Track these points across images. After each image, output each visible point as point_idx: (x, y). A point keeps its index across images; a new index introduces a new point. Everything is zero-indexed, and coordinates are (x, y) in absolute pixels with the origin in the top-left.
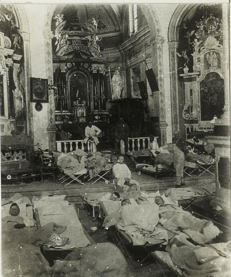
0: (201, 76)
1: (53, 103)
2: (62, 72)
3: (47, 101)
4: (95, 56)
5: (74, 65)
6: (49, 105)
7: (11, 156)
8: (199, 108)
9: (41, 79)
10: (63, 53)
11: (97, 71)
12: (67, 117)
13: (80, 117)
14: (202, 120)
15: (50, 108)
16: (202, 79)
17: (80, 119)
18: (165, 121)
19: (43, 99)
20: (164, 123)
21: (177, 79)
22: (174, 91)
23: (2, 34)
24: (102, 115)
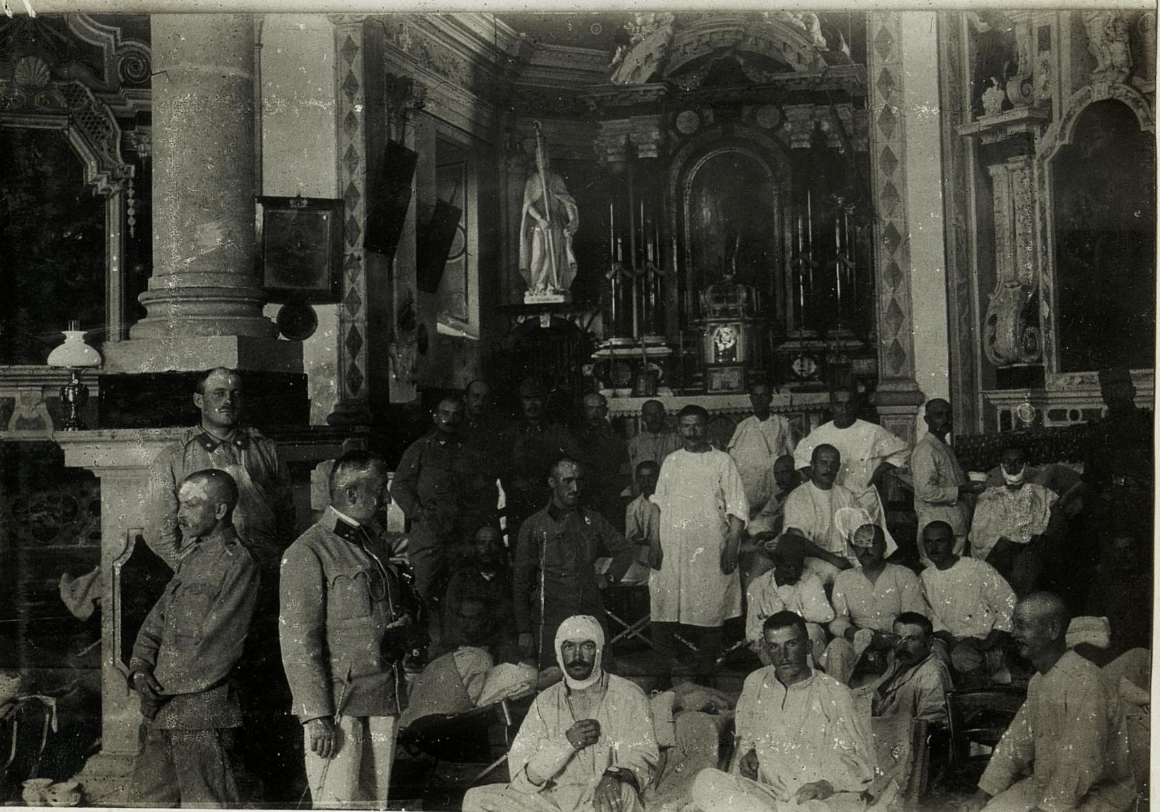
0: (1055, 127)
1: (363, 305)
2: (644, 159)
3: (334, 295)
4: (797, 66)
5: (711, 119)
6: (347, 313)
7: (60, 525)
8: (1049, 304)
9: (305, 202)
10: (644, 68)
11: (812, 138)
12: (655, 367)
13: (717, 364)
14: (1064, 369)
15: (348, 326)
16: (1058, 144)
17: (717, 375)
18: (913, 380)
19: (315, 288)
20: (903, 387)
21: (971, 152)
22: (961, 217)
23: (110, 32)
24: (824, 352)
